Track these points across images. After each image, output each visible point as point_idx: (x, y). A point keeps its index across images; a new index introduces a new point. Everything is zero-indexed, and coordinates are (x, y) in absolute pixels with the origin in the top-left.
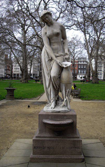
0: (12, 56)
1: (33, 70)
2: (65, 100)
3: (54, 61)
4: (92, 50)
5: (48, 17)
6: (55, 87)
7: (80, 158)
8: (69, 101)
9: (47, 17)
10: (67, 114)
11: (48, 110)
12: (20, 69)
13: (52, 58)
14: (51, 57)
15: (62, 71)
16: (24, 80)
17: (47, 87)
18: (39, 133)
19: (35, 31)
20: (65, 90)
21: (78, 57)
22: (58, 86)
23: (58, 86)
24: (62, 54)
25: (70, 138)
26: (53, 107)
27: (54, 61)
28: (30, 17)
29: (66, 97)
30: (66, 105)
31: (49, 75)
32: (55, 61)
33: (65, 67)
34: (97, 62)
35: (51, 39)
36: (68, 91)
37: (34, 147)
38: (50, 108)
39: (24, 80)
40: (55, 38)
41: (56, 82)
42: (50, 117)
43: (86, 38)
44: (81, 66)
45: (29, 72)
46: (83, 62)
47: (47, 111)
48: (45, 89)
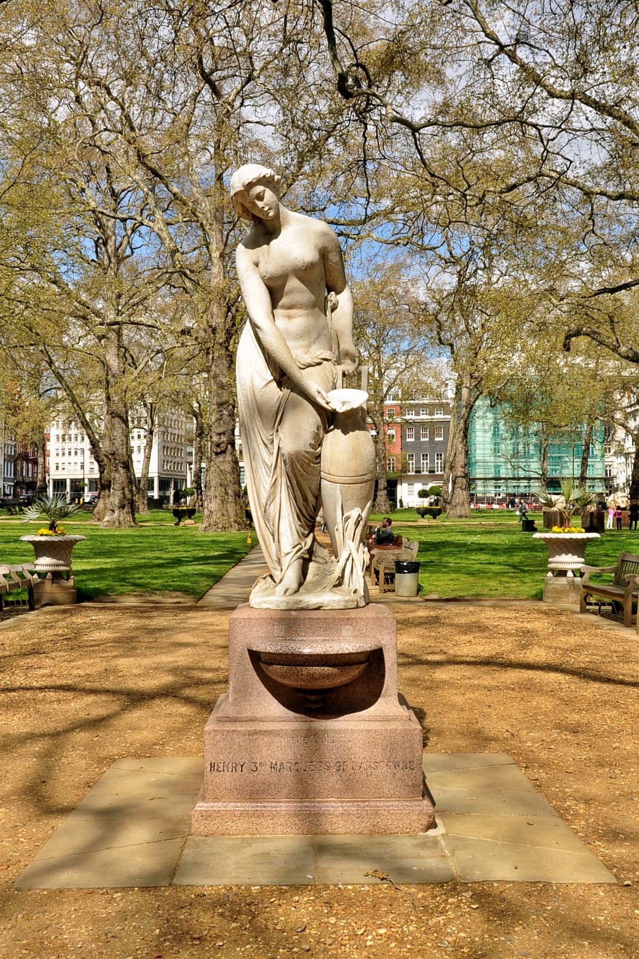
1: (162, 463)
21: (401, 385)
23: (311, 499)
43: (143, 324)
44: (417, 433)
46: (432, 414)
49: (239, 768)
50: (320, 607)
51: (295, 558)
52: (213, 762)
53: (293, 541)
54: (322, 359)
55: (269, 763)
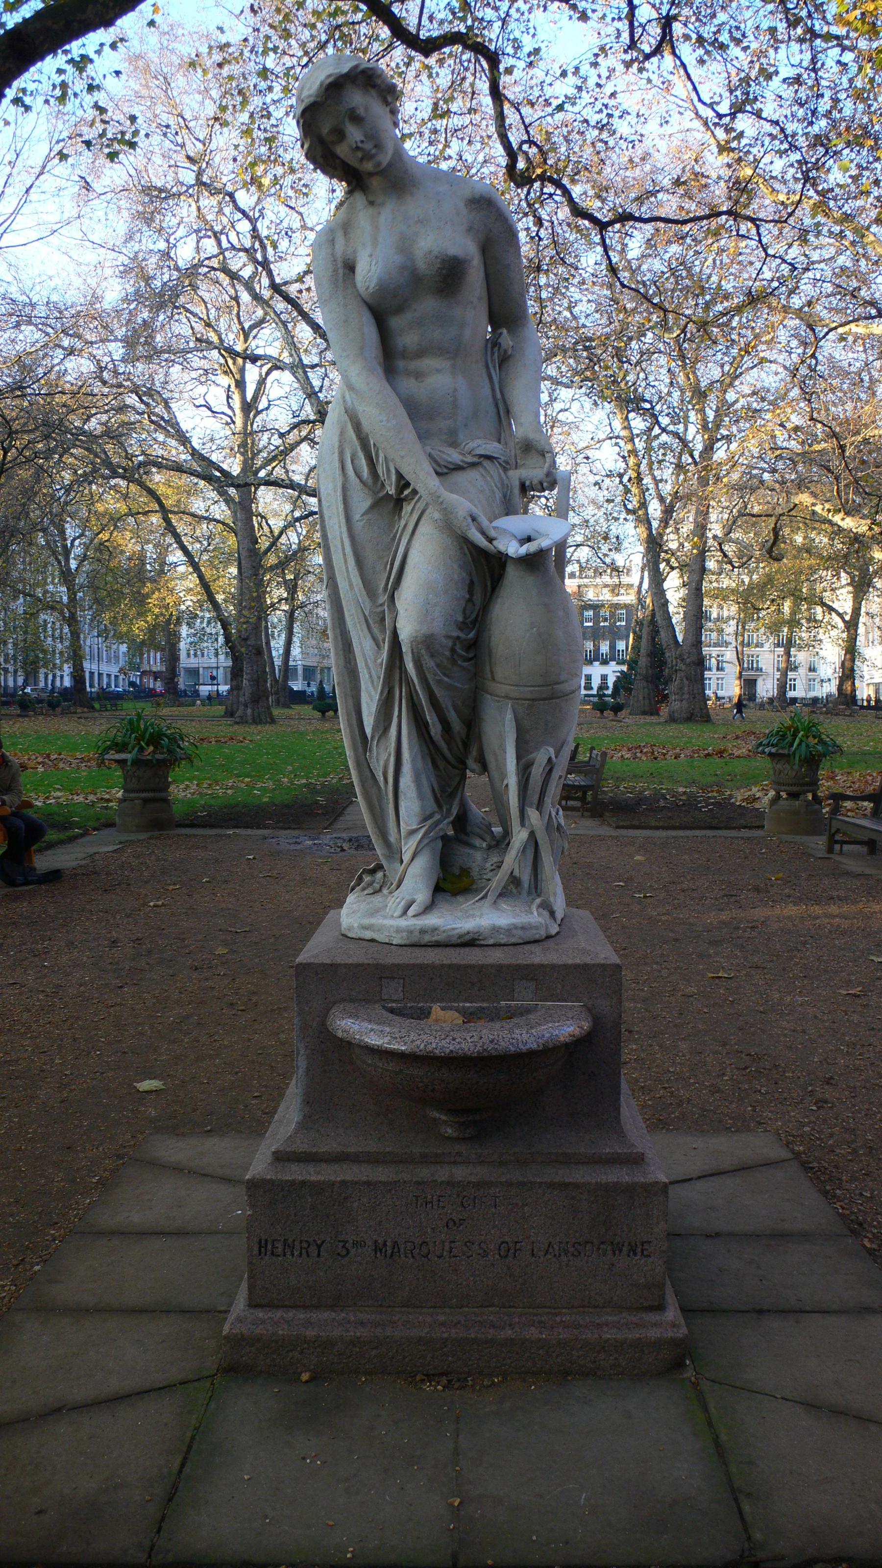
0: (171, 559)
2: (520, 836)
3: (420, 506)
4: (668, 511)
5: (361, 112)
6: (436, 729)
7: (653, 1334)
8: (552, 842)
9: (356, 118)
10: (537, 956)
11: (377, 921)
12: (221, 639)
13: (403, 483)
14: (400, 476)
15: (494, 589)
16: (246, 706)
17: (368, 730)
18: (303, 1126)
19: (311, 394)
20: (519, 758)
22: (457, 725)
23: (457, 725)
24: (492, 448)
25: (567, 1160)
26: (422, 896)
27: (420, 506)
28: (281, 305)
29: (533, 814)
30: (526, 877)
31: (383, 630)
32: (436, 499)
33: (523, 550)
34: (699, 589)
35: (396, 322)
36: (541, 757)
37: (262, 1245)
38: (394, 902)
39: (246, 706)
40: (428, 305)
41: (439, 682)
42: (393, 990)
45: (278, 662)
47: (368, 935)
48: (355, 749)
49: (313, 1251)
50: (474, 940)
51: (426, 841)
52: (263, 1238)
53: (423, 808)
54: (481, 456)
55: (370, 1243)
